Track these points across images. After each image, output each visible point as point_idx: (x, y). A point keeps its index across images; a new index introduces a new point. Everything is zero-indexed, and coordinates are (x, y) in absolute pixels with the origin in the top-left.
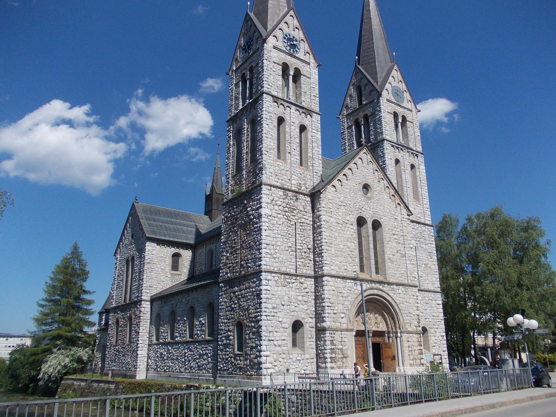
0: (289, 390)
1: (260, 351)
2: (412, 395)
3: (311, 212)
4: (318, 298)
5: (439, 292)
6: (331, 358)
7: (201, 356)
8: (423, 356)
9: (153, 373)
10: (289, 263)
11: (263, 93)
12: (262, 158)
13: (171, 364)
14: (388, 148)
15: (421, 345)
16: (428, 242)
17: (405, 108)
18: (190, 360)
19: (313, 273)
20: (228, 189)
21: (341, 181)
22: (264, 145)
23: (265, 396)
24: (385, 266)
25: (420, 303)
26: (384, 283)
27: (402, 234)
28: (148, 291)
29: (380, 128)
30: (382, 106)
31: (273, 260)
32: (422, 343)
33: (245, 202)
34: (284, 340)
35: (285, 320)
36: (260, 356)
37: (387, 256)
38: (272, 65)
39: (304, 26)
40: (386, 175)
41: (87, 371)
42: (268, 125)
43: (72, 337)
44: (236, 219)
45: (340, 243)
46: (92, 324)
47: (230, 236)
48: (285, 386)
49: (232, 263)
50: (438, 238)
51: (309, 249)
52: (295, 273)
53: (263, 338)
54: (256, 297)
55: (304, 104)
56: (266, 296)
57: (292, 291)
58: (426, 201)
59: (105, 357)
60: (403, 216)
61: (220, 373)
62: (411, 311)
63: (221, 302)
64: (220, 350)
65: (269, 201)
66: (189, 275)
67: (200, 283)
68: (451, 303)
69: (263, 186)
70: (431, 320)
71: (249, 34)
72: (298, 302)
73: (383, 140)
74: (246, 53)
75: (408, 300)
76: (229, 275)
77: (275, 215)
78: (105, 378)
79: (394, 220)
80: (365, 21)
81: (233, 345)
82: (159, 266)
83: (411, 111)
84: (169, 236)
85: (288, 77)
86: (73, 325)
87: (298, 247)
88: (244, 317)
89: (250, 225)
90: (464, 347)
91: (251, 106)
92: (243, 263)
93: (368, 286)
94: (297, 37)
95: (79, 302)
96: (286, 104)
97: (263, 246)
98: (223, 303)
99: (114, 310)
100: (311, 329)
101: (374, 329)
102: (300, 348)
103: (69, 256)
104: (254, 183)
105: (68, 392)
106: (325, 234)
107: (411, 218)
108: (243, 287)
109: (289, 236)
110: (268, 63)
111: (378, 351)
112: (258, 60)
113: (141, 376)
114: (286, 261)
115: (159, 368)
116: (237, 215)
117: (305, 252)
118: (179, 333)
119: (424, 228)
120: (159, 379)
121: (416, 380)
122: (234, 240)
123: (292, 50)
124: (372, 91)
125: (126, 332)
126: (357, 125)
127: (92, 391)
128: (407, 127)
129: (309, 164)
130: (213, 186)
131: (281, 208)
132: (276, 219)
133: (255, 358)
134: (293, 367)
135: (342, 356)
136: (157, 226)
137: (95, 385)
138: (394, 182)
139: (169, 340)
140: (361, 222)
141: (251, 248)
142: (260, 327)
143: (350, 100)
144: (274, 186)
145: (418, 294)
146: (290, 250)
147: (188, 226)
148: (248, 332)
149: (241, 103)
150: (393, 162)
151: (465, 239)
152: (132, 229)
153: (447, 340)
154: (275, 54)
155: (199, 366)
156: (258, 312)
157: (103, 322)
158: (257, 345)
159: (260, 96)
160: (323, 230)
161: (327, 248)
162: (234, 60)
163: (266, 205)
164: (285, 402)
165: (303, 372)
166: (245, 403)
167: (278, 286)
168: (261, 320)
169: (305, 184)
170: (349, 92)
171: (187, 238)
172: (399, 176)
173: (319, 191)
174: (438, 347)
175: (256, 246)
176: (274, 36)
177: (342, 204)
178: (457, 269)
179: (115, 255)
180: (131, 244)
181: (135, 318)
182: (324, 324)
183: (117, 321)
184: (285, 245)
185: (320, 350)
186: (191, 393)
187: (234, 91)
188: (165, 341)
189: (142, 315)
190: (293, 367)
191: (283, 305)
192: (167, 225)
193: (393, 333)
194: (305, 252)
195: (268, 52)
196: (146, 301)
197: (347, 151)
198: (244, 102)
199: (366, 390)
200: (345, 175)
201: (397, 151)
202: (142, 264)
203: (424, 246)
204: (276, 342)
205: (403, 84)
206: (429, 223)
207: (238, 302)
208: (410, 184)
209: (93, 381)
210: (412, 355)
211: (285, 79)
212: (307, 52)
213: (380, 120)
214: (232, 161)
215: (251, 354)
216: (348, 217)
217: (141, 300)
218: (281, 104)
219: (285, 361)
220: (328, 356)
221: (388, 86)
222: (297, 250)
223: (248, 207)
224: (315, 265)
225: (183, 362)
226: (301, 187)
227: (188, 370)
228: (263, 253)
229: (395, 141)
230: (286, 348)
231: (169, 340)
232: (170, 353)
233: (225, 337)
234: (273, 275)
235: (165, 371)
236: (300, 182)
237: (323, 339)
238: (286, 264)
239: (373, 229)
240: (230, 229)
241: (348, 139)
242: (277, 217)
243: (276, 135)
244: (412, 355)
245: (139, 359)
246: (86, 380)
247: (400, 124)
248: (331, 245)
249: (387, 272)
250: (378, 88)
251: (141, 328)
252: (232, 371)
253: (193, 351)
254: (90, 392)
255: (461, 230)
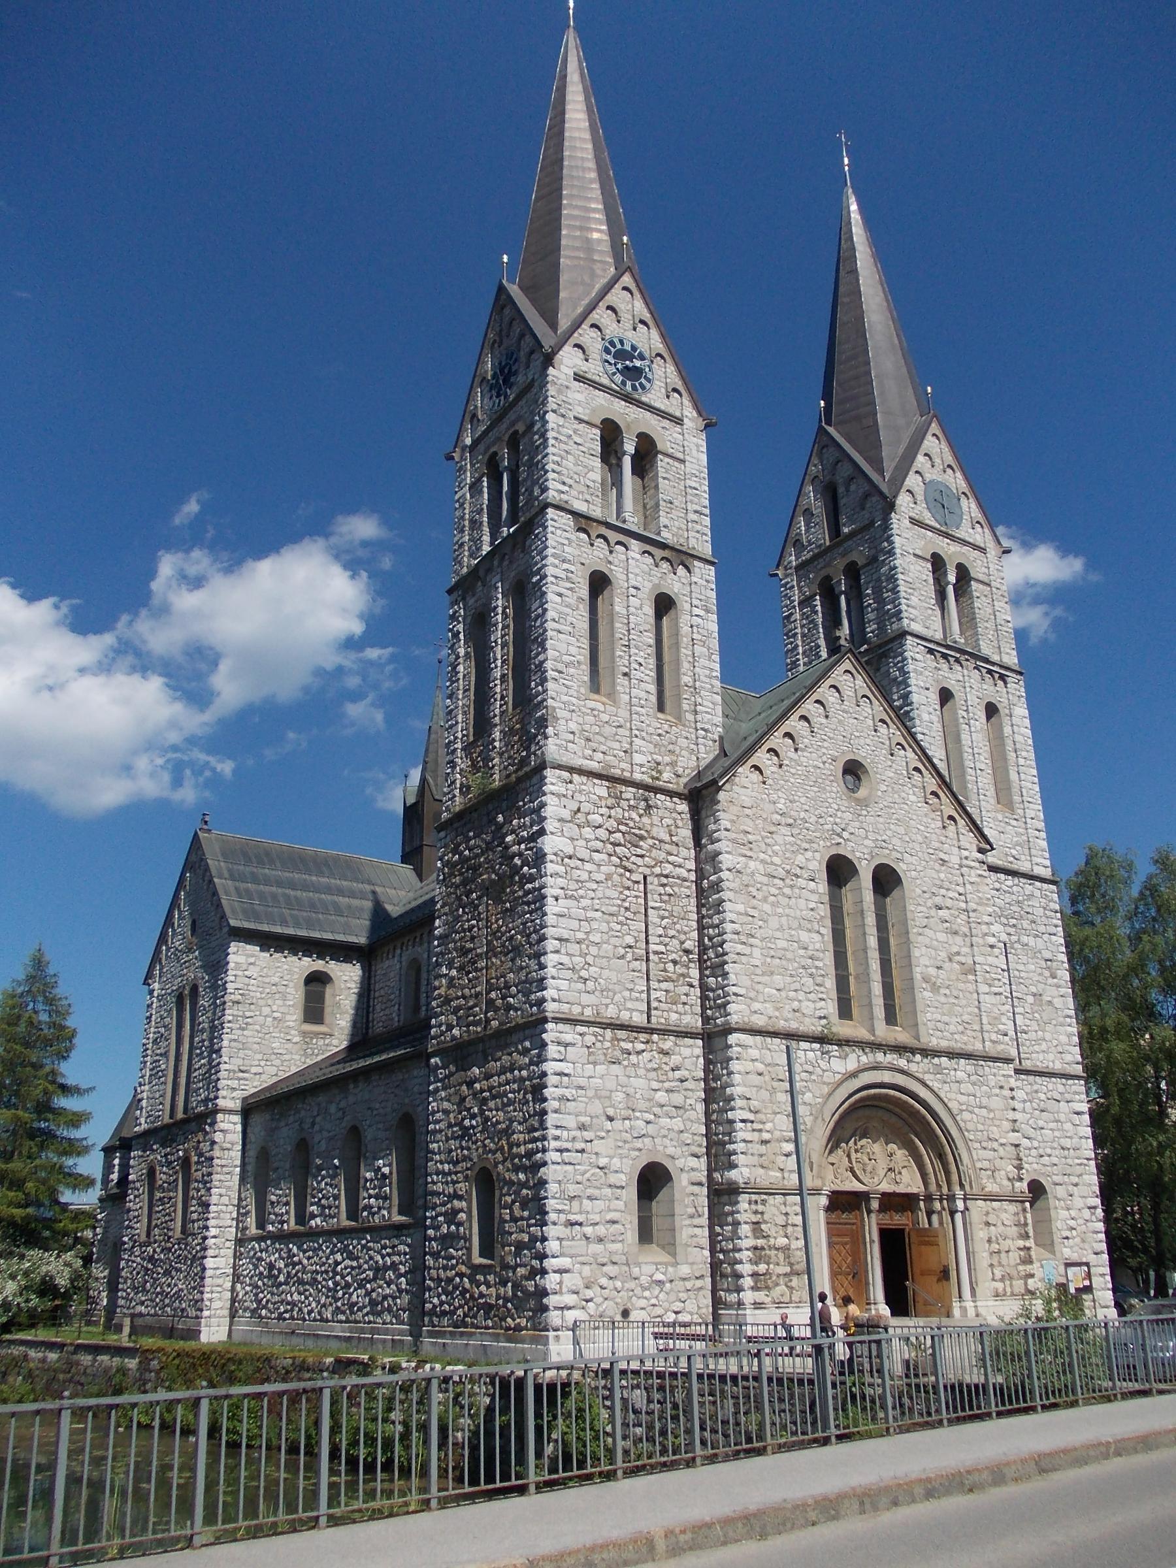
0: (623, 1372)
1: (542, 1256)
2: (1000, 1391)
3: (690, 843)
4: (716, 1096)
5: (1078, 1077)
6: (754, 1275)
7: (379, 1271)
8: (1035, 1268)
9: (248, 1324)
10: (627, 994)
11: (547, 505)
12: (545, 691)
13: (296, 1297)
14: (918, 656)
15: (1026, 1236)
16: (1042, 929)
17: (965, 543)
18: (348, 1285)
19: (700, 1023)
20: (453, 782)
21: (777, 755)
22: (551, 653)
23: (553, 1394)
24: (914, 1001)
25: (1024, 1111)
26: (913, 1051)
27: (963, 905)
28: (235, 1084)
29: (893, 602)
30: (896, 539)
31: (580, 986)
32: (1030, 1229)
33: (500, 818)
34: (614, 1222)
35: (616, 1163)
36: (543, 1272)
37: (918, 969)
38: (570, 427)
39: (662, 316)
40: (913, 736)
41: (69, 1319)
42: (560, 595)
43: (27, 1219)
44: (475, 869)
45: (778, 934)
46: (82, 1183)
47: (457, 919)
48: (612, 1364)
49: (464, 997)
50: (1075, 919)
51: (687, 952)
52: (644, 1023)
53: (552, 1216)
54: (529, 1097)
55: (666, 536)
56: (559, 1092)
57: (637, 1076)
58: (1035, 809)
59: (119, 1276)
60: (966, 853)
61: (431, 1321)
62: (995, 1132)
63: (434, 1113)
64: (432, 1254)
65: (566, 814)
66: (353, 1035)
67: (377, 1059)
68: (1115, 1110)
69: (548, 772)
70: (1055, 1160)
71: (506, 342)
72: (657, 1110)
73: (903, 634)
74: (498, 396)
75: (985, 1101)
76: (456, 1032)
77: (585, 854)
78: (112, 1339)
79: (937, 867)
80: (843, 299)
81: (468, 1239)
82: (266, 1010)
83: (983, 550)
84: (297, 925)
85: (620, 460)
86: (29, 1185)
87: (652, 947)
88: (499, 1155)
89: (512, 884)
90: (1159, 1241)
91: (514, 546)
92: (493, 995)
93: (864, 1059)
94: (643, 347)
95: (46, 1120)
96: (613, 536)
97: (551, 944)
98: (439, 1116)
99: (141, 1140)
100: (696, 1189)
101: (886, 1187)
102: (663, 1248)
103: (20, 990)
104: (524, 762)
105: (11, 1379)
106: (734, 908)
107: (991, 858)
108: (494, 1066)
109: (628, 914)
110: (561, 421)
111: (902, 1255)
112: (533, 414)
113: (214, 1331)
114: (617, 988)
115: (265, 1307)
116: (477, 856)
117: (675, 962)
118: (318, 1204)
119: (1029, 888)
120: (265, 1340)
121: (998, 1345)
122: (470, 930)
123: (629, 383)
124: (867, 496)
125: (174, 1205)
126: (822, 591)
127: (77, 1378)
128: (971, 597)
129: (685, 707)
130: (423, 780)
131: (602, 833)
132: (588, 866)
133: (528, 1278)
134: (643, 1303)
135: (788, 1269)
136: (262, 896)
137: (86, 1359)
138: (938, 754)
139: (291, 1225)
140: (839, 871)
141: (517, 951)
142: (543, 1183)
143: (807, 525)
144: (581, 772)
145: (1013, 1082)
146: (629, 956)
147: (352, 894)
148: (509, 1199)
149: (486, 538)
150: (934, 698)
151: (1154, 919)
152: (192, 905)
153: (1107, 1220)
154: (579, 397)
155: (373, 1303)
156: (535, 1140)
157: (115, 1177)
158: (534, 1239)
159: (537, 515)
160: (725, 895)
161: (740, 948)
162: (468, 417)
163: (557, 825)
164: (611, 1408)
165: (670, 1317)
166: (505, 1410)
167: (595, 1063)
168: (545, 1164)
169: (673, 764)
170: (804, 502)
171: (347, 929)
172: (951, 736)
173: (714, 782)
174: (1078, 1240)
175: (531, 945)
176: (576, 345)
177: (783, 821)
178: (1133, 1009)
179: (146, 983)
180: (190, 950)
181: (198, 1163)
182: (733, 1174)
183: (151, 1173)
184: (613, 941)
185: (722, 1251)
186: (321, 1389)
187: (467, 506)
188: (281, 1230)
189: (217, 1153)
190: (643, 1303)
191: (611, 1119)
192: (292, 893)
193: (941, 1200)
194: (675, 962)
195: (559, 392)
196: (231, 1112)
197: (801, 668)
198: (493, 537)
199: (852, 1372)
200: (788, 735)
201: (945, 666)
202: (218, 1007)
203: (1031, 941)
204: (588, 1230)
205: (959, 474)
206: (1046, 873)
207: (482, 1112)
208: (984, 761)
209: (79, 1346)
210: (1000, 1264)
211: (610, 466)
212: (675, 390)
213: (892, 579)
214: (464, 701)
215: (517, 1265)
216: (800, 860)
217: (216, 1111)
218: (599, 536)
219: (618, 1284)
220: (745, 1269)
221: (912, 481)
222: (652, 956)
223: (506, 835)
224: (704, 998)
225: (329, 1290)
226: (660, 772)
227: (343, 1313)
228: (550, 964)
229: (939, 636)
230: (618, 1246)
231: (291, 1225)
232: (294, 1264)
233: (444, 1214)
234: (579, 1029)
235: (280, 1318)
236: (659, 758)
237: (730, 1219)
238: (618, 997)
239: (874, 892)
240: (459, 898)
241: (803, 635)
242: (591, 861)
243: (584, 626)
244: (1000, 1264)
245: (208, 1281)
246: (61, 1346)
247: (950, 589)
248: (752, 941)
249: (921, 1018)
250: (884, 488)
251: (213, 1191)
252: (465, 1315)
253: (357, 1258)
254: (70, 1381)
255: (1141, 893)
